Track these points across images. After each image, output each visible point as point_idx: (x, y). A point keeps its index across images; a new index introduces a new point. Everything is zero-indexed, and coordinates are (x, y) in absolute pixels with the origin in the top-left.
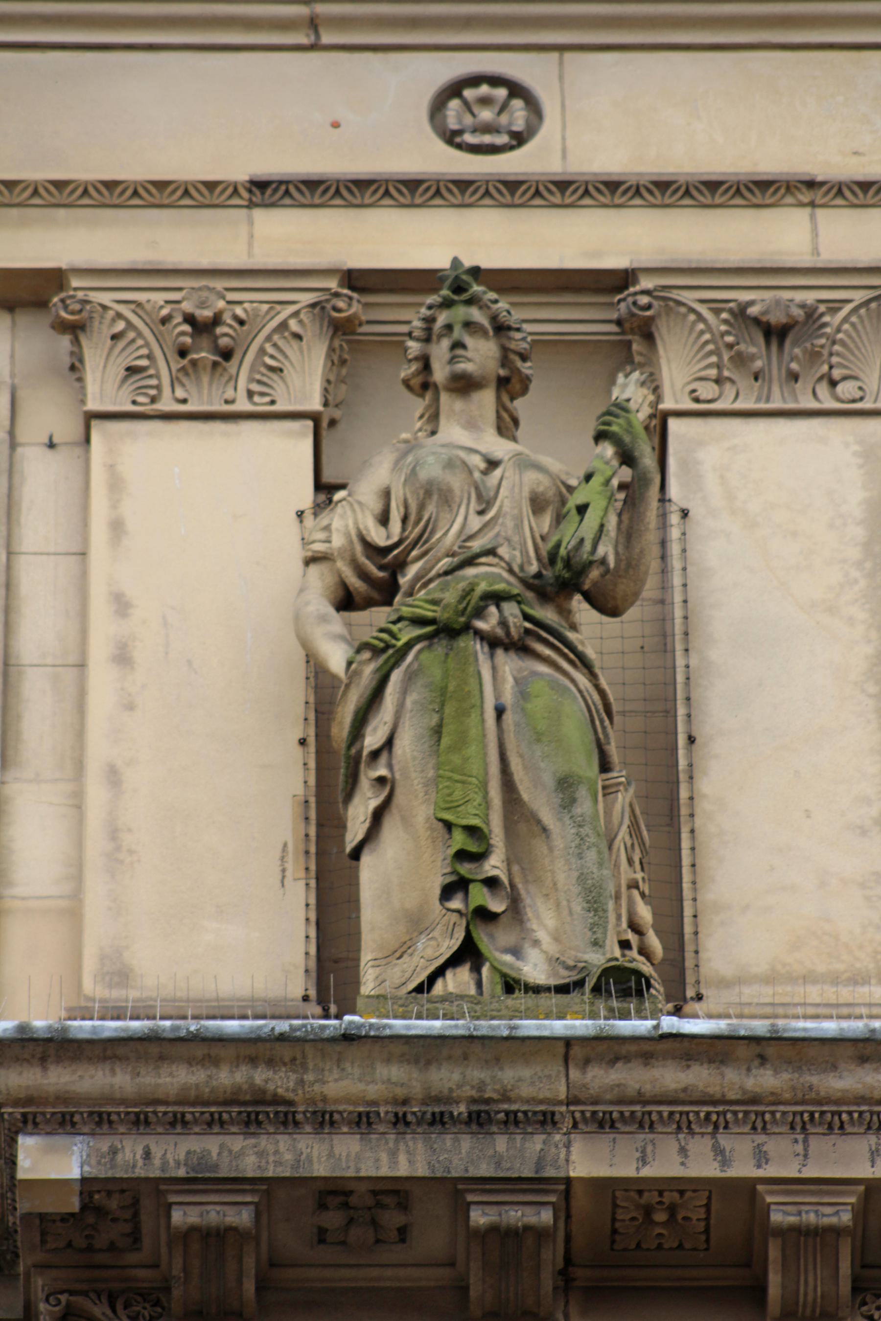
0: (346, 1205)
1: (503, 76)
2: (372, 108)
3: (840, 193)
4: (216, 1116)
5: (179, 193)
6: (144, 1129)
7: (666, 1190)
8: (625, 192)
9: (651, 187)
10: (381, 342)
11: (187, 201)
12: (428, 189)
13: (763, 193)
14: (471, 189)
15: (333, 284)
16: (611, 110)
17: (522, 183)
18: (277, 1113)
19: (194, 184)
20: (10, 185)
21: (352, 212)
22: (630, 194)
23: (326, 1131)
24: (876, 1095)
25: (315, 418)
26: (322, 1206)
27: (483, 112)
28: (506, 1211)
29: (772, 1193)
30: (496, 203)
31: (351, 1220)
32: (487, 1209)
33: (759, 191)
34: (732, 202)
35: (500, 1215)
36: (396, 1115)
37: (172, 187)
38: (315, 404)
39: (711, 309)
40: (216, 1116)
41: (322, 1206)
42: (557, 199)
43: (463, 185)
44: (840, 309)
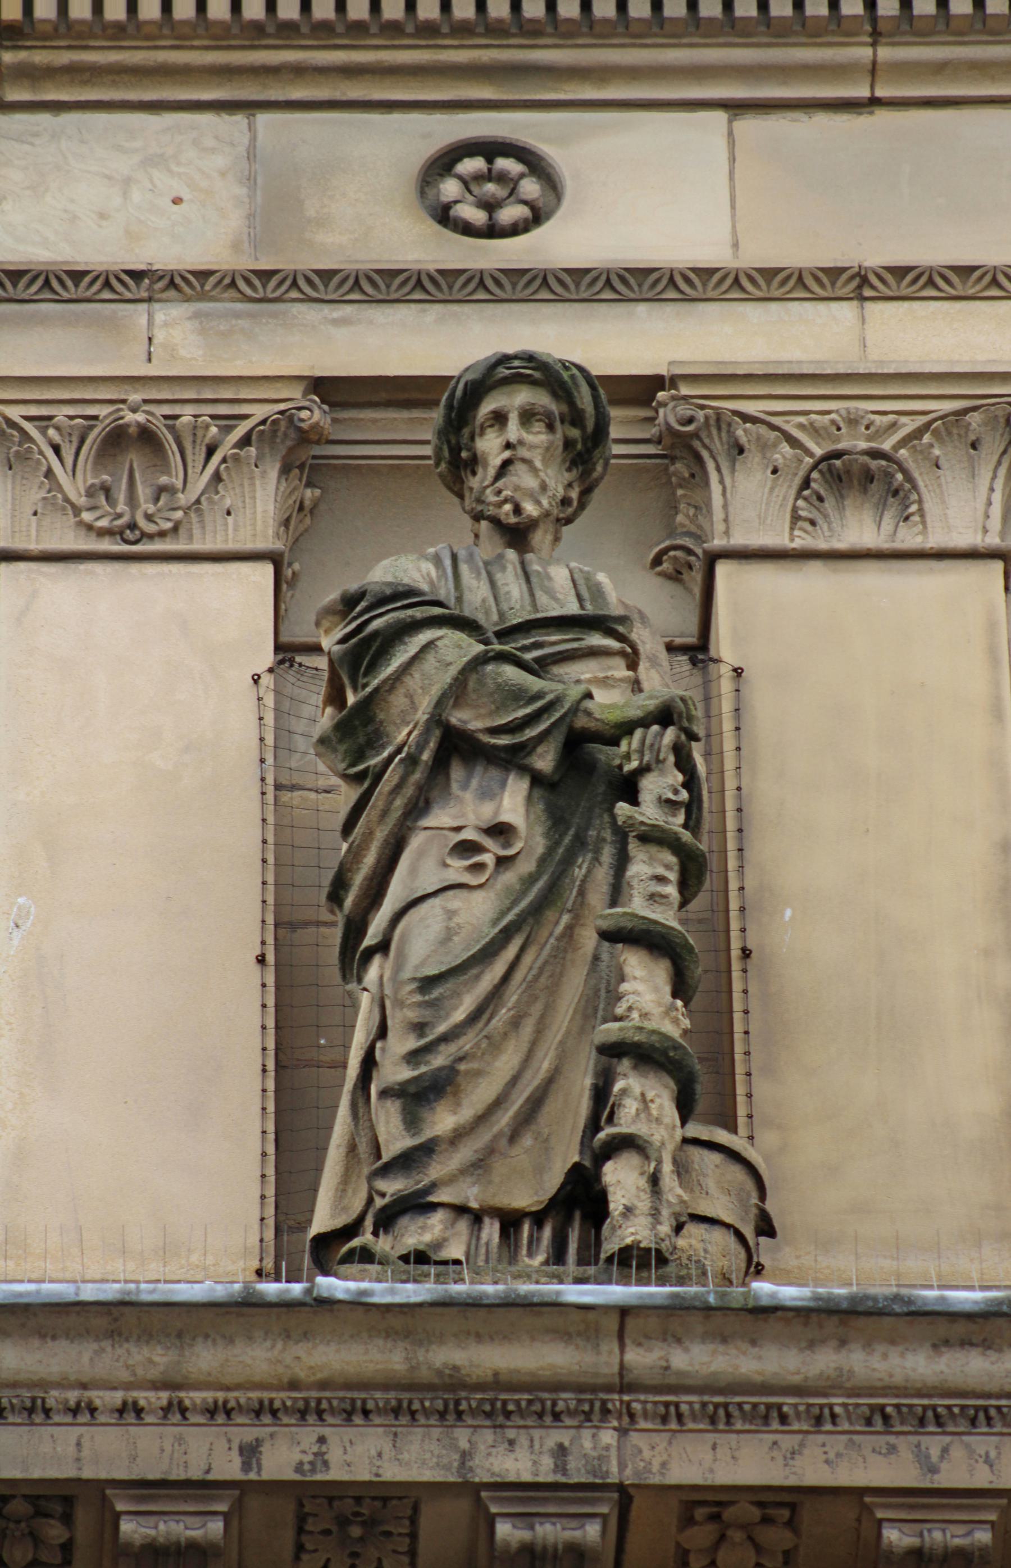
0: (715, 1517)
1: (514, 142)
2: (361, 179)
3: (931, 283)
4: (359, 1403)
5: (600, 284)
6: (553, 1422)
7: (392, 1498)
8: (784, 282)
9: (754, 274)
10: (398, 466)
11: (355, 296)
12: (595, 279)
13: (964, 283)
14: (909, 277)
15: (296, 392)
16: (647, 183)
17: (25, 272)
18: (704, 1405)
19: (554, 273)
20: (15, 275)
21: (821, 308)
22: (34, 288)
23: (220, 1421)
24: (1008, 1388)
25: (276, 559)
26: (688, 1521)
27: (493, 186)
28: (929, 1531)
29: (494, 1499)
30: (301, 296)
31: (722, 1537)
32: (907, 1527)
33: (858, 284)
34: (925, 293)
35: (921, 1535)
36: (261, 1402)
37: (977, 274)
38: (267, 540)
39: (36, 427)
40: (359, 1403)
41: (688, 1521)
42: (72, 293)
43: (450, 275)
44: (235, 426)
